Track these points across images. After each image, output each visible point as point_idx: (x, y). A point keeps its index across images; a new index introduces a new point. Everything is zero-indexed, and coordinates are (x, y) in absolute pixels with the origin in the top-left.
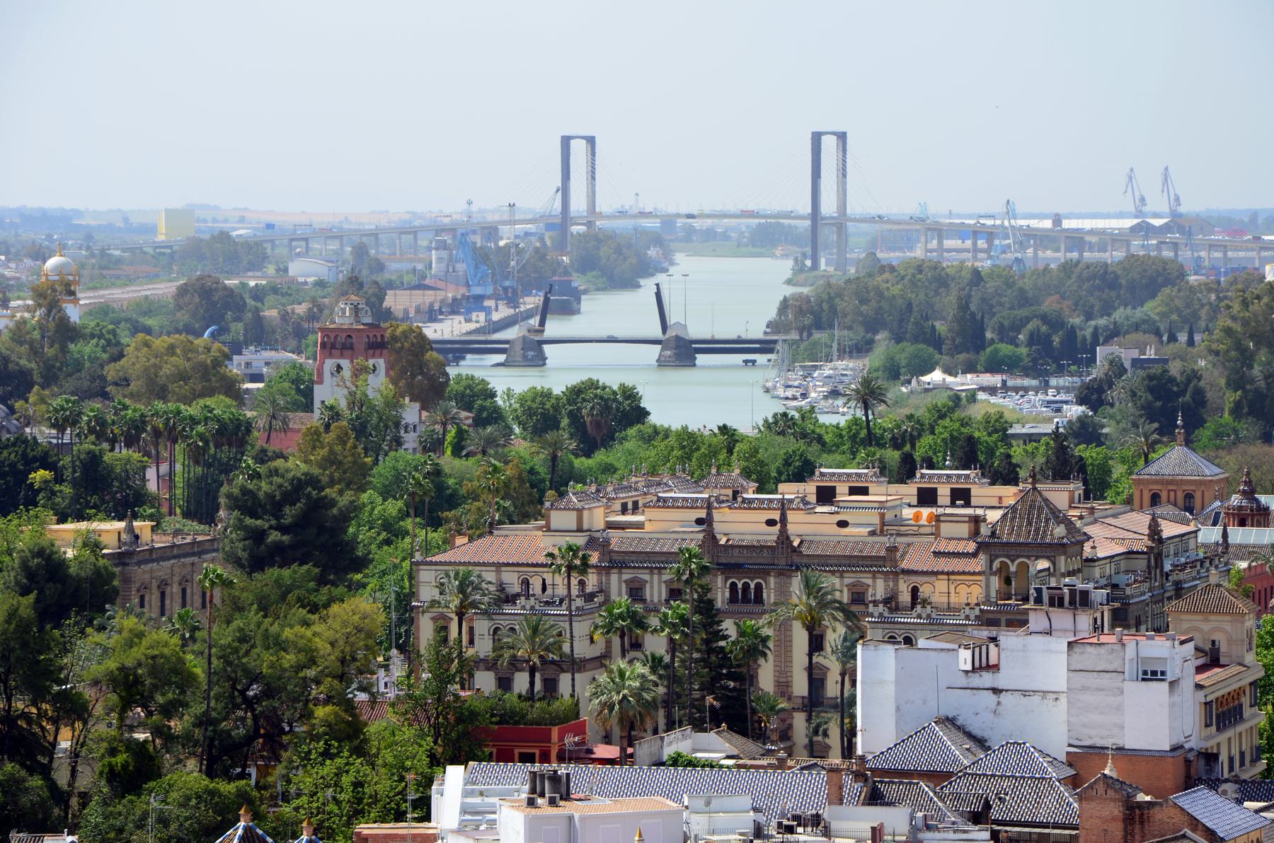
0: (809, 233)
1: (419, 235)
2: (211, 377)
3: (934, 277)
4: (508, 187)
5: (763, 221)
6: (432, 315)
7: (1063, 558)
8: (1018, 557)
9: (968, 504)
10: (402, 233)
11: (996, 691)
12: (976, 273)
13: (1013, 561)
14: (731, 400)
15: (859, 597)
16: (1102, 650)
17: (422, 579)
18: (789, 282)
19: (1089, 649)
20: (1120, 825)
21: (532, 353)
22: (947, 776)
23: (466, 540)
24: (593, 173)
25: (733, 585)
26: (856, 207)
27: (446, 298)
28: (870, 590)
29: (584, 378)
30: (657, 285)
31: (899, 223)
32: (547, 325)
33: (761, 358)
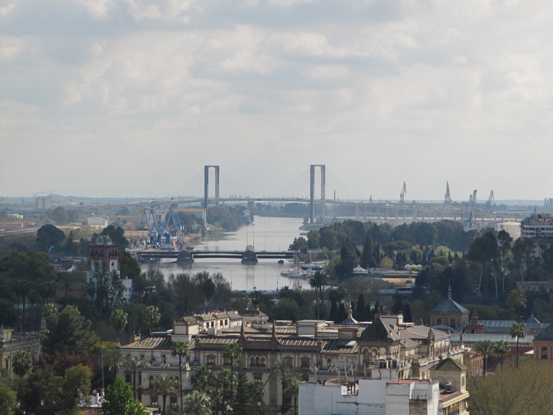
4: (181, 185)
8: (372, 346)
10: (137, 206)
11: (356, 404)
13: (370, 348)
14: (269, 280)
15: (305, 363)
16: (401, 386)
18: (300, 228)
21: (185, 258)
24: (218, 181)
25: (252, 359)
28: (310, 360)
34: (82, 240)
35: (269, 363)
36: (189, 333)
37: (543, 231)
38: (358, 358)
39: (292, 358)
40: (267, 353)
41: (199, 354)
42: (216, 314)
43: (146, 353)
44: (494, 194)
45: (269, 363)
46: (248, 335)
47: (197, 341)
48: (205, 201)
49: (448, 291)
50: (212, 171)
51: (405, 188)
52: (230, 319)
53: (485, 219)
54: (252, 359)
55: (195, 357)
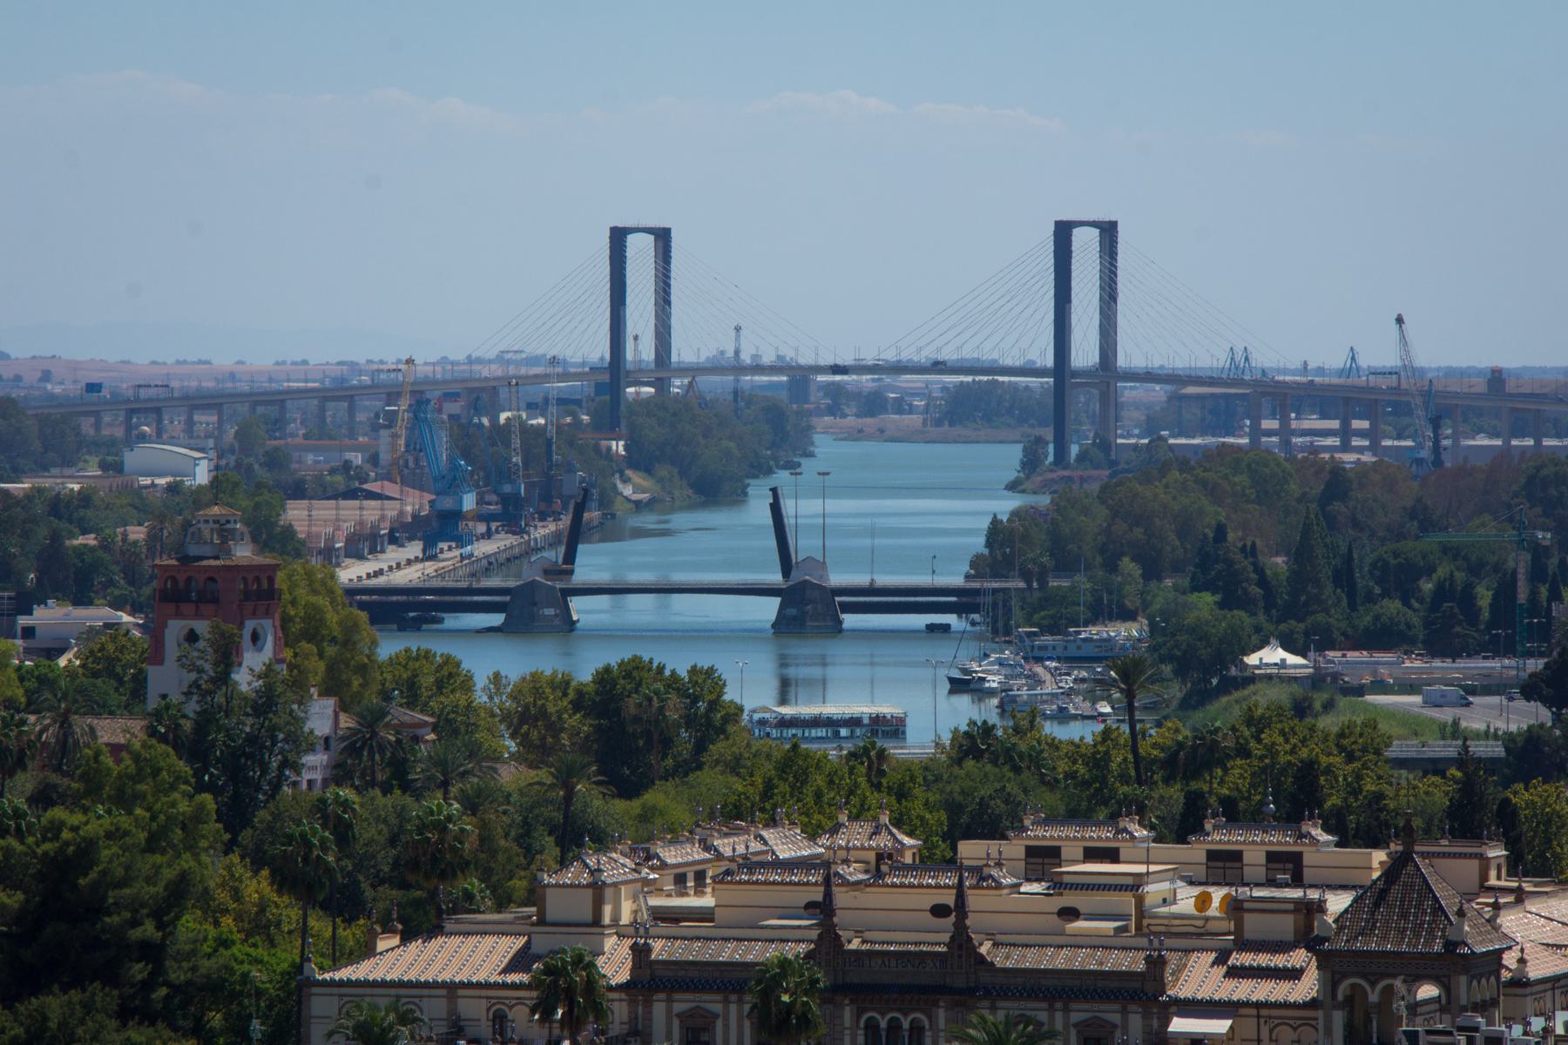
0: (1051, 401)
1: (289, 404)
3: (1261, 477)
4: (495, 300)
5: (969, 379)
6: (364, 543)
7: (1463, 979)
9: (1297, 881)
10: (255, 404)
12: (1337, 471)
13: (1373, 984)
14: (918, 701)
17: (314, 1012)
18: (1013, 486)
21: (533, 608)
23: (396, 941)
27: (401, 513)
28: (1118, 1033)
29: (627, 656)
30: (774, 491)
31: (1211, 381)
32: (578, 560)
39: (1115, 1026)
40: (936, 1004)
41: (648, 1003)
43: (425, 1003)
48: (616, 369)
50: (1085, 243)
54: (871, 1027)
55: (633, 1019)
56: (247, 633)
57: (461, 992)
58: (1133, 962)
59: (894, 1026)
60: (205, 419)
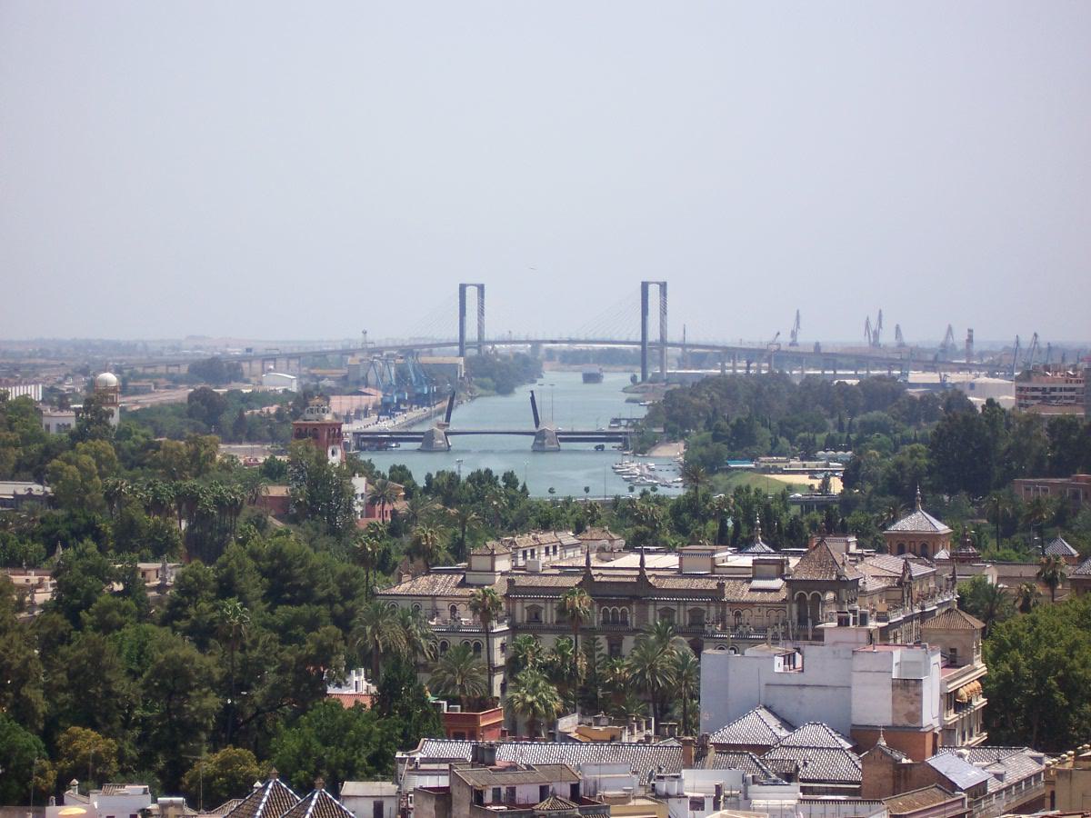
2: (199, 463)
3: (726, 386)
4: (412, 316)
6: (362, 413)
18: (625, 390)
19: (867, 655)
20: (891, 780)
22: (767, 748)
26: (673, 335)
33: (608, 446)
34: (990, 402)
35: (634, 618)
36: (496, 570)
37: (1053, 394)
38: (787, 610)
42: (539, 536)
43: (423, 603)
44: (902, 328)
45: (634, 618)
46: (597, 572)
47: (511, 582)
49: (916, 495)
50: (654, 291)
51: (798, 323)
52: (562, 546)
53: (838, 372)
56: (330, 451)
57: (437, 598)
58: (713, 585)
59: (614, 612)
60: (293, 363)
